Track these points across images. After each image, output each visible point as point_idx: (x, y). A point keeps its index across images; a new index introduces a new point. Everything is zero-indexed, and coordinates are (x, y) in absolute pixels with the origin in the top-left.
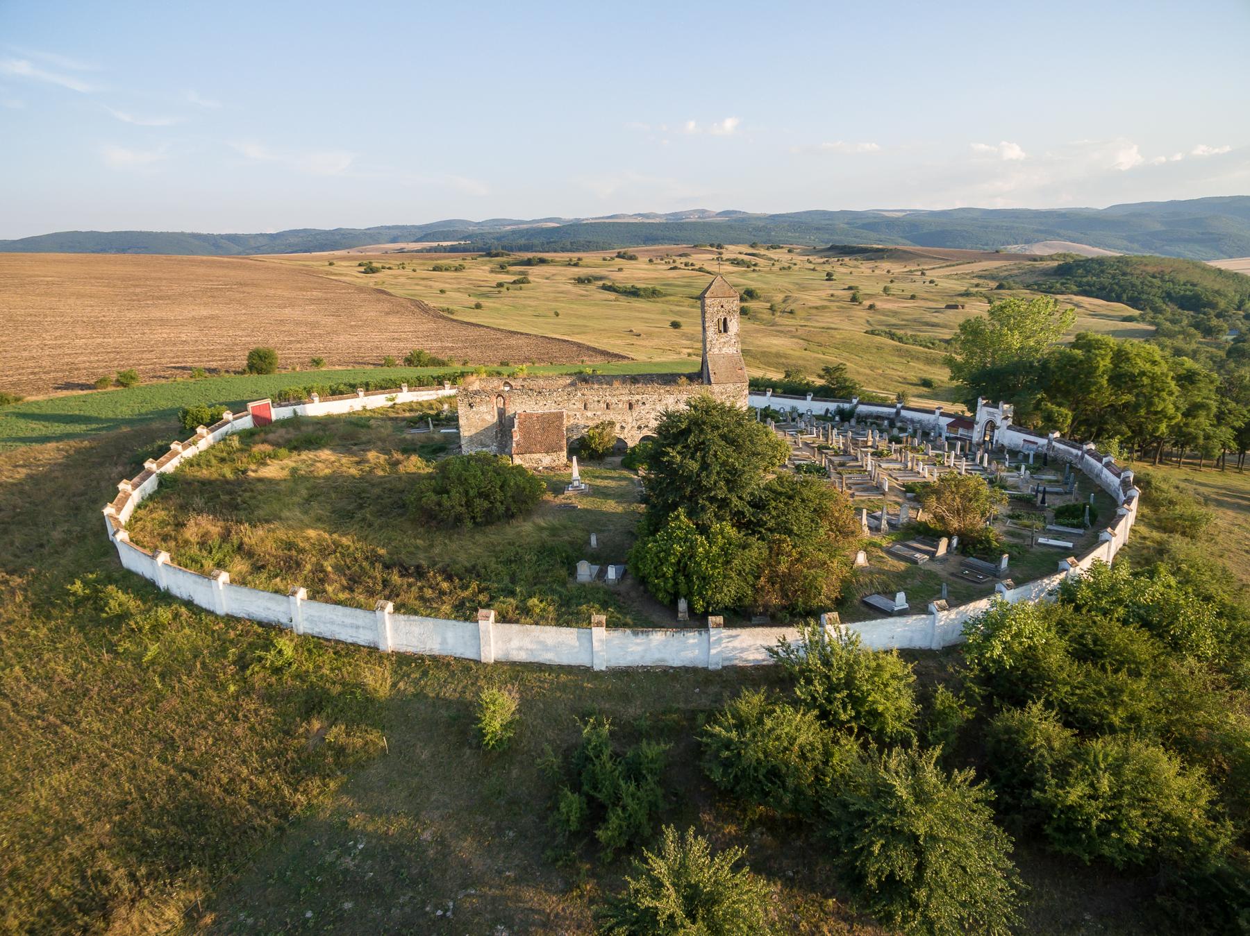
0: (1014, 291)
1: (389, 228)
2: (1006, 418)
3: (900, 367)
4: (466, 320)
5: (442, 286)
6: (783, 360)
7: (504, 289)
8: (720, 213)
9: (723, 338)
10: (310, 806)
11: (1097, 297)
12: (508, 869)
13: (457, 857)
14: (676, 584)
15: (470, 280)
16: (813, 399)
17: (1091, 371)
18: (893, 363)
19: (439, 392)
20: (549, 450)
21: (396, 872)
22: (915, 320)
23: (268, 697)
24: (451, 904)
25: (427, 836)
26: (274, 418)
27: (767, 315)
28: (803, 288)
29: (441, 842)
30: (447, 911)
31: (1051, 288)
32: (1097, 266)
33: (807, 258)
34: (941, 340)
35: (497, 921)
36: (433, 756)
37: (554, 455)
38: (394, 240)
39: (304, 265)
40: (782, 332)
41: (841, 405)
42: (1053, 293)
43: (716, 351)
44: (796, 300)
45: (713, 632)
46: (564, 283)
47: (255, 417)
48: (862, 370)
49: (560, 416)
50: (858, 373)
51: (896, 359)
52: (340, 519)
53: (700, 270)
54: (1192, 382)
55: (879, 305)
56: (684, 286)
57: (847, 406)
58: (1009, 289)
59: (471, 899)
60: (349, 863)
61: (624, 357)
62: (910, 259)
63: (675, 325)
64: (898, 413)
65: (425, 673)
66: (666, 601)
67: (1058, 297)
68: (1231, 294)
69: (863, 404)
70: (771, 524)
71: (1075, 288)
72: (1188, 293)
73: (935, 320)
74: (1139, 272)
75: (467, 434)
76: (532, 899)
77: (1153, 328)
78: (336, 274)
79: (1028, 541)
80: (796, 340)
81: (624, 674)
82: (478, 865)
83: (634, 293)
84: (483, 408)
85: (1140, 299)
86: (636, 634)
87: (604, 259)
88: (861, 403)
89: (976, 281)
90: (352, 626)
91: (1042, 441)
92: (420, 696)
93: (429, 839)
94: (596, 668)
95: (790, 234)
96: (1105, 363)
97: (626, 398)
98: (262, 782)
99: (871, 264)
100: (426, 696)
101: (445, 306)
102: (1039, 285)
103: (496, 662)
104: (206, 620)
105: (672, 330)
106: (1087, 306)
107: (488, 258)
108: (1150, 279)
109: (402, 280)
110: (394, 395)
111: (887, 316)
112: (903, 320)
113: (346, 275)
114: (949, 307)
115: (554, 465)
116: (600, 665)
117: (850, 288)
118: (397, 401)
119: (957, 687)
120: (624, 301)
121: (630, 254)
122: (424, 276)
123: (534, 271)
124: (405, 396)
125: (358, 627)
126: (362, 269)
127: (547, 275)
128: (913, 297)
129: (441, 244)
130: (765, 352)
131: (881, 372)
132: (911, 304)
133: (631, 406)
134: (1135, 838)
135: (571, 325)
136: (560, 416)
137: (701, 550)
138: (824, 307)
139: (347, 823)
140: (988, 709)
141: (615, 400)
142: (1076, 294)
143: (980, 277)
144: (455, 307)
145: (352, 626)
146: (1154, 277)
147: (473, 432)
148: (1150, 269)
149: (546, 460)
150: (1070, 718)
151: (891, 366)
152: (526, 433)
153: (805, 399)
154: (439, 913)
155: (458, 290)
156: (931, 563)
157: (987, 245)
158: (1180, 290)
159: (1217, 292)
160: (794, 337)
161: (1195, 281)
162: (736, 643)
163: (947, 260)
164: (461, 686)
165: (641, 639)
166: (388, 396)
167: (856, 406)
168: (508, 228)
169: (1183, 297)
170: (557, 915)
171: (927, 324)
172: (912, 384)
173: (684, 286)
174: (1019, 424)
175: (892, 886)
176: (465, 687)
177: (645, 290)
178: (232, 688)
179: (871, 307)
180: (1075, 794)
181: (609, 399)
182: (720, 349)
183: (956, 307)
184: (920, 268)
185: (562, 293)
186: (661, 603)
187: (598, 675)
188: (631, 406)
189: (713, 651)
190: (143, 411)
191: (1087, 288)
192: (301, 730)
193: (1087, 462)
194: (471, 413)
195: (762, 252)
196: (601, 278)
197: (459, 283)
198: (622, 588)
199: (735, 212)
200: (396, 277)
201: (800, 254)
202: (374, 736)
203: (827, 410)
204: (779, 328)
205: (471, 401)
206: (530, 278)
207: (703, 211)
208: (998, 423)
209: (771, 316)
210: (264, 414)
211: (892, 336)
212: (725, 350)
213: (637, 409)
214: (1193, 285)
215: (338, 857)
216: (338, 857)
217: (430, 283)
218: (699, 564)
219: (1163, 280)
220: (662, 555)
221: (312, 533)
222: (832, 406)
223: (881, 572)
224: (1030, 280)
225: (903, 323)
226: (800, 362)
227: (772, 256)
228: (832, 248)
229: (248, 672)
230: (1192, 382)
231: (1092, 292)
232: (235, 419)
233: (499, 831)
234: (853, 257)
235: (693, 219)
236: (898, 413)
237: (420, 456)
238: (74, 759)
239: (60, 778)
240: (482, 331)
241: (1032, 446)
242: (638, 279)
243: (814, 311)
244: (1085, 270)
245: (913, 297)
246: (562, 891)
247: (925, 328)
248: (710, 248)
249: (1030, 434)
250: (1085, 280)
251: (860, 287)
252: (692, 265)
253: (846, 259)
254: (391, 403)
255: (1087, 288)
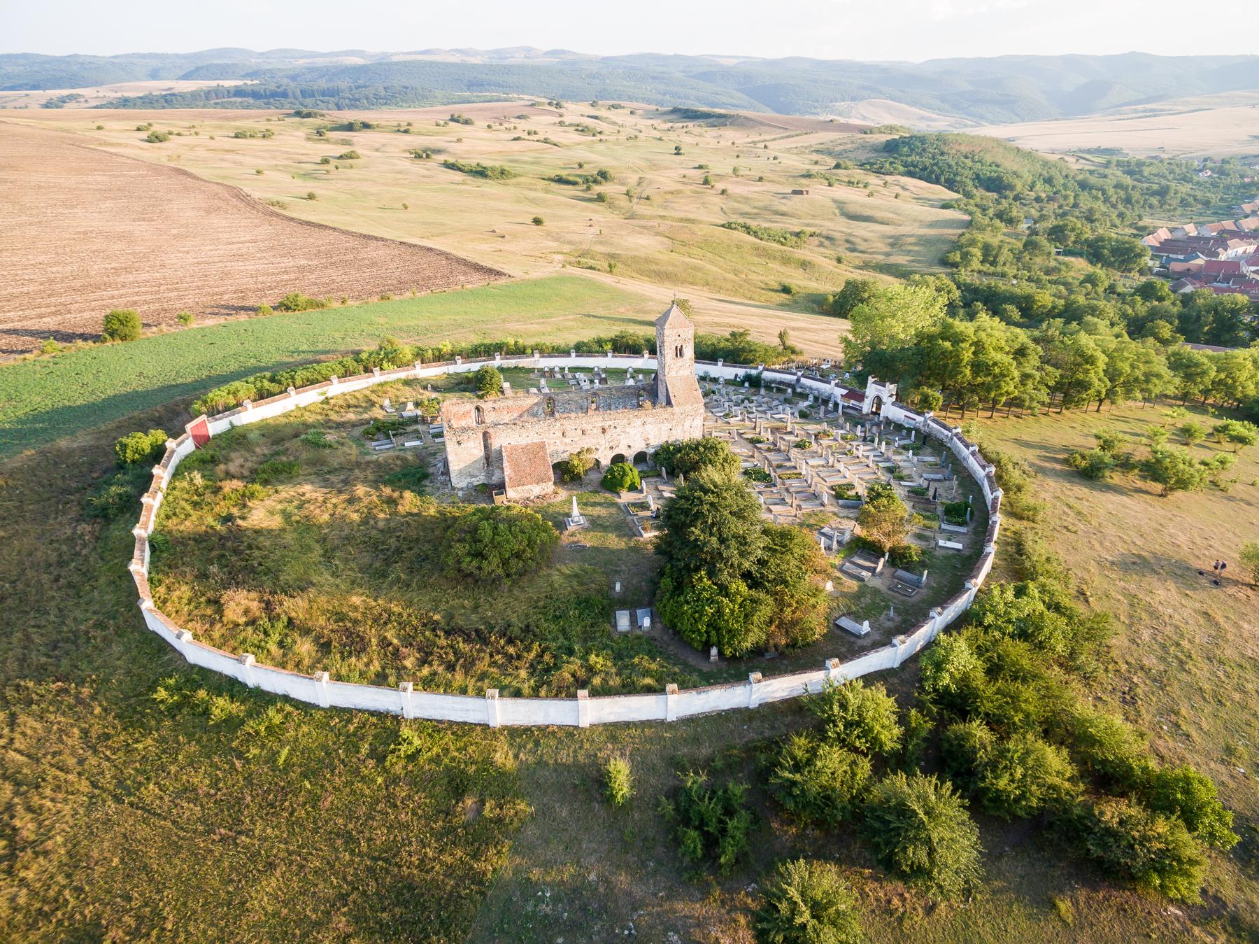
0: (850, 172)
1: (144, 56)
2: (891, 396)
3: (760, 269)
4: (305, 217)
5: (261, 163)
6: (654, 267)
7: (331, 167)
8: (547, 53)
9: (680, 361)
10: (495, 870)
11: (920, 178)
12: (660, 891)
13: (620, 889)
14: (709, 636)
15: (286, 153)
16: (723, 365)
17: (958, 363)
18: (753, 264)
19: (369, 380)
20: (540, 480)
21: (583, 909)
22: (765, 208)
23: (415, 782)
24: (631, 924)
25: (592, 877)
26: (211, 434)
27: (623, 202)
28: (655, 166)
29: (603, 879)
30: (630, 930)
31: (881, 168)
32: (920, 144)
33: (650, 122)
34: (791, 234)
35: (666, 930)
36: (571, 813)
37: (544, 485)
38: (154, 75)
39: (63, 130)
40: (644, 227)
41: (748, 371)
42: (883, 174)
43: (673, 374)
44: (650, 183)
45: (754, 685)
46: (399, 158)
47: (195, 437)
48: (727, 275)
49: (542, 446)
50: (725, 279)
51: (756, 260)
52: (376, 577)
53: (546, 141)
54: (1024, 355)
55: (731, 189)
56: (533, 163)
57: (754, 372)
58: (845, 169)
59: (643, 917)
60: (545, 909)
61: (499, 274)
62: (752, 127)
63: (537, 222)
64: (798, 380)
65: (537, 743)
66: (700, 648)
67: (888, 178)
68: (1026, 175)
69: (767, 370)
70: (771, 577)
71: (901, 169)
72: (993, 174)
73: (784, 209)
74: (954, 151)
75: (456, 468)
76: (683, 910)
77: (967, 218)
78: (111, 145)
79: (933, 544)
80: (661, 238)
81: (690, 721)
82: (638, 891)
83: (481, 173)
84: (471, 444)
85: (955, 181)
86: (699, 693)
87: (438, 125)
88: (765, 369)
89: (815, 157)
90: (462, 710)
91: (920, 419)
92: (541, 763)
93: (595, 879)
94: (669, 720)
95: (625, 83)
96: (967, 356)
97: (600, 424)
98: (449, 860)
99: (714, 132)
100: (547, 764)
101: (275, 198)
102: (871, 164)
103: (592, 726)
104: (318, 715)
105: (535, 227)
106: (912, 189)
107: (297, 119)
108: (962, 159)
109: (202, 153)
110: (325, 389)
111: (739, 202)
112: (755, 208)
113: (126, 146)
114: (795, 192)
115: (543, 493)
116: (671, 717)
117: (700, 167)
118: (329, 395)
119: (920, 706)
120: (474, 184)
121: (465, 116)
122: (227, 147)
123: (360, 137)
124: (337, 388)
125: (468, 710)
126: (144, 135)
127: (377, 146)
128: (761, 179)
129: (221, 83)
130: (635, 256)
131: (744, 276)
132: (759, 187)
133: (604, 431)
134: (1034, 802)
135: (425, 223)
136: (542, 446)
137: (727, 610)
138: (679, 192)
139: (529, 878)
140: (942, 723)
141: (589, 427)
142: (902, 175)
143: (817, 151)
144: (282, 198)
145: (462, 710)
146: (966, 157)
147: (462, 465)
148: (964, 149)
149: (536, 490)
150: (993, 722)
151: (753, 269)
152: (516, 466)
153: (716, 365)
154: (626, 932)
155: (276, 168)
156: (873, 578)
157: (817, 101)
158: (987, 172)
159: (1015, 173)
160: (657, 234)
161: (999, 162)
162: (770, 689)
163: (787, 129)
164: (571, 750)
165: (703, 696)
166: (320, 391)
167: (761, 373)
168: (302, 62)
169: (989, 179)
170: (704, 918)
171: (777, 213)
172: (773, 290)
173: (533, 163)
174: (900, 400)
175: (919, 872)
176: (575, 751)
177: (493, 169)
178: (380, 780)
179: (723, 192)
180: (1002, 783)
181: (585, 426)
182: (677, 372)
183: (800, 193)
184: (762, 138)
185: (400, 172)
186: (696, 650)
187: (671, 726)
188: (604, 431)
189: (754, 697)
190: (20, 413)
191: (912, 169)
192: (459, 809)
193: (955, 444)
194: (459, 449)
195: (603, 113)
196: (438, 151)
197: (274, 158)
198: (656, 634)
199: (563, 52)
200: (192, 148)
201: (643, 117)
202: (522, 806)
203: (736, 375)
204: (643, 222)
205: (459, 439)
206: (359, 151)
207: (529, 49)
208: (884, 400)
209: (628, 203)
210: (202, 432)
211: (747, 229)
212: (682, 372)
213: (609, 432)
214: (997, 166)
215: (535, 906)
216: (535, 906)
217: (238, 158)
218: (727, 621)
219: (973, 161)
220: (697, 615)
221: (356, 600)
222: (741, 372)
223: (844, 595)
224: (863, 156)
225: (756, 211)
226: (670, 268)
227: (615, 119)
228: (675, 111)
229: (388, 764)
230: (1024, 355)
231: (915, 173)
232: (179, 445)
233: (643, 864)
234: (696, 122)
235: (519, 59)
236: (798, 380)
237: (412, 491)
238: (271, 866)
239: (271, 883)
240: (331, 237)
241: (911, 421)
242: (482, 153)
243: (669, 196)
244: (910, 148)
245: (761, 179)
246: (701, 899)
247: (778, 218)
248: (549, 108)
249: (909, 411)
250: (909, 159)
251: (711, 165)
252: (535, 133)
253: (690, 124)
254: (323, 397)
255: (912, 169)
